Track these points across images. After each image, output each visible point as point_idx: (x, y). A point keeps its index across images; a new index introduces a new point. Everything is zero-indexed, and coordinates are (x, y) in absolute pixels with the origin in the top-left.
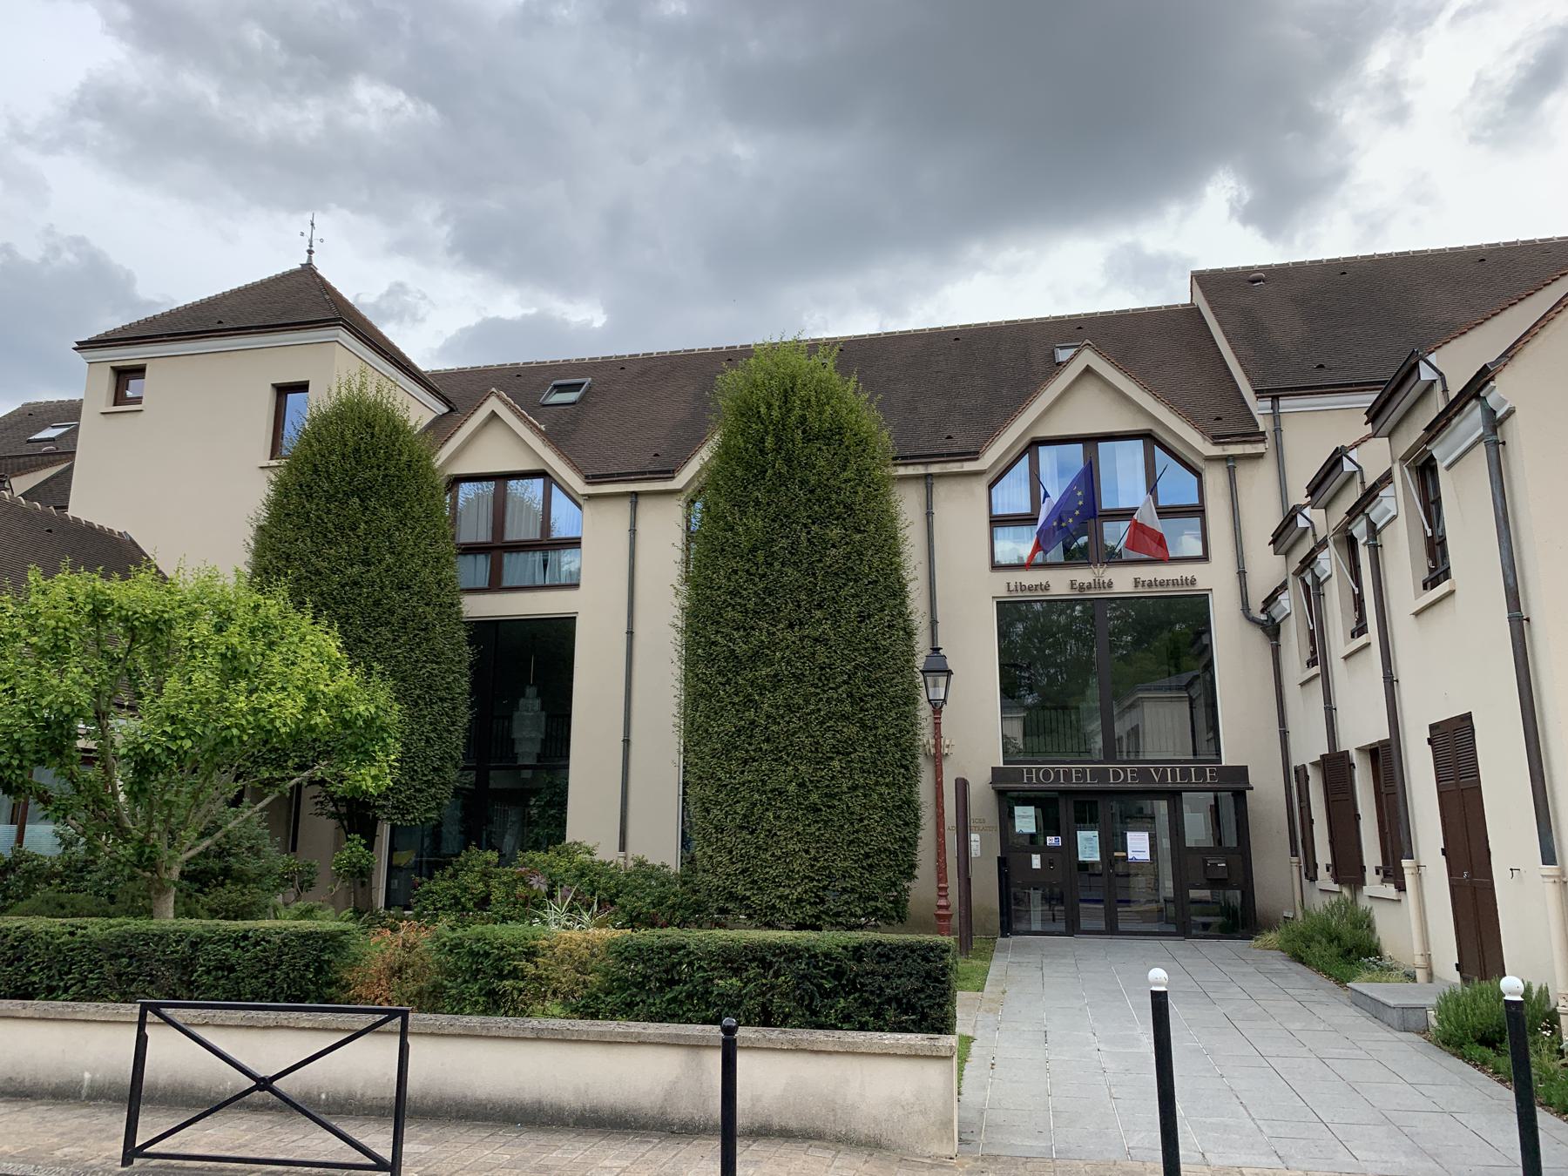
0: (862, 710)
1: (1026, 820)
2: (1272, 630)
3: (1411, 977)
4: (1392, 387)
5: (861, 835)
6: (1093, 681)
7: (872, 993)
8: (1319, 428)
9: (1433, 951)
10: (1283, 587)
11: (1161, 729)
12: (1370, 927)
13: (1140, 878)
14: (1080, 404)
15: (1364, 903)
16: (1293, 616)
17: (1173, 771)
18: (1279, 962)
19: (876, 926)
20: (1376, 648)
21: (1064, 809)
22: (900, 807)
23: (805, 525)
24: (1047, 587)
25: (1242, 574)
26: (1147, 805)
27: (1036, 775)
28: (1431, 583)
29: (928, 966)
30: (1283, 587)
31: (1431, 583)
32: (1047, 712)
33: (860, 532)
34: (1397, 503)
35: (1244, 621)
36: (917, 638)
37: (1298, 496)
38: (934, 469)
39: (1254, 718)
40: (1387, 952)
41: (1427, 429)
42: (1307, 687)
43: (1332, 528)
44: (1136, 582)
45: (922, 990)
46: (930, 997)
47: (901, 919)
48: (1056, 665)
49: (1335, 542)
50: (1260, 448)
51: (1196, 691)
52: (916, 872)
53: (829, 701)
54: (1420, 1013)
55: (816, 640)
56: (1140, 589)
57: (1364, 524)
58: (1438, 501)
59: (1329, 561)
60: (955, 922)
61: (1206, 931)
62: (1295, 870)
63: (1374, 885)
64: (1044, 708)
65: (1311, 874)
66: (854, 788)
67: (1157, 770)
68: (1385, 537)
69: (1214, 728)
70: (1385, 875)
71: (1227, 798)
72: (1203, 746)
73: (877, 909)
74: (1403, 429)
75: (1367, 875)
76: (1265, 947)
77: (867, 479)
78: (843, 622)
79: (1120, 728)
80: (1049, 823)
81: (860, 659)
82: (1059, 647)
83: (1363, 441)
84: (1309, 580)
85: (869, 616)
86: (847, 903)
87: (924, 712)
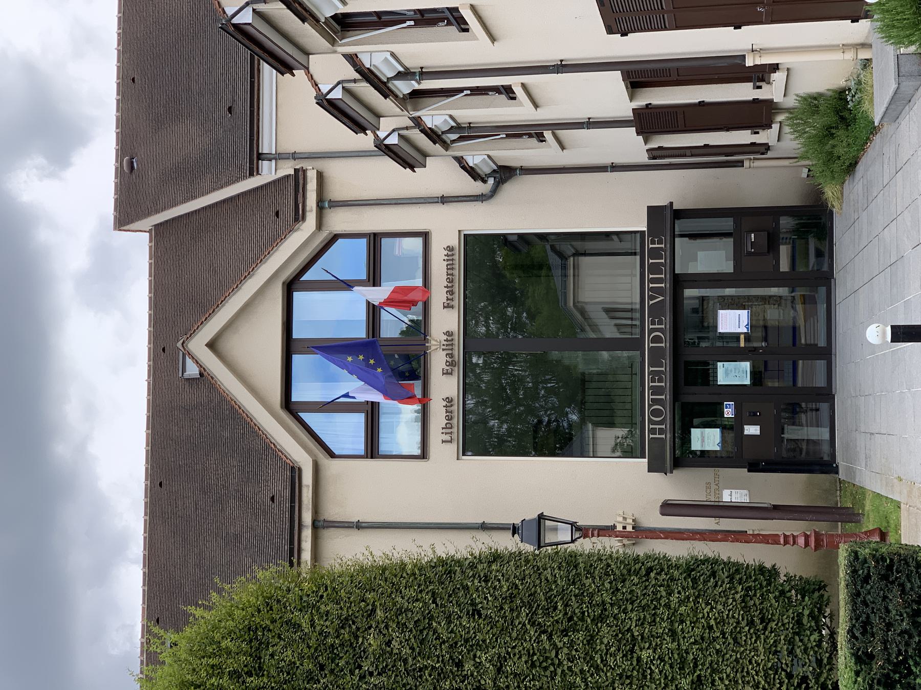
0: (582, 619)
1: (707, 439)
2: (505, 174)
3: (867, 64)
4: (257, 50)
5: (728, 629)
6: (555, 355)
7: (907, 644)
8: (292, 116)
9: (840, 42)
10: (460, 160)
11: (609, 286)
12: (816, 97)
13: (768, 317)
14: (246, 352)
15: (791, 102)
16: (491, 153)
17: (652, 281)
18: (856, 187)
19: (831, 616)
20: (529, 79)
21: (694, 398)
22: (695, 581)
23: (362, 677)
24: (449, 400)
25: (444, 200)
26: (688, 305)
27: (657, 425)
28: (462, 25)
29: (874, 578)
30: (460, 160)
31: (462, 25)
32: (589, 399)
33: (374, 611)
34: (377, 51)
35: (492, 201)
36: (501, 549)
37: (366, 141)
38: (307, 518)
39: (600, 194)
40: (841, 83)
41: (303, 20)
42: (566, 144)
43: (399, 114)
44: (447, 306)
45: (902, 585)
46: (909, 577)
47: (821, 587)
48: (536, 388)
49: (415, 110)
50: (312, 176)
51: (568, 249)
52: (768, 565)
53: (571, 659)
54: (903, 60)
55: (499, 670)
56: (455, 303)
57: (397, 83)
58: (379, 14)
59: (436, 116)
60: (822, 527)
61: (826, 253)
62: (757, 163)
63: (773, 91)
64: (583, 403)
65: (763, 149)
66: (673, 633)
67: (651, 298)
68: (413, 64)
69: (607, 235)
70: (763, 80)
71: (681, 225)
72: (626, 246)
73: (811, 615)
74: (303, 41)
75: (761, 97)
76: (841, 198)
77: (313, 600)
78: (479, 636)
79: (609, 331)
80: (709, 415)
81: (523, 618)
82: (517, 381)
83: (311, 78)
84: (454, 136)
85: (473, 604)
86: (805, 651)
87: (585, 545)
